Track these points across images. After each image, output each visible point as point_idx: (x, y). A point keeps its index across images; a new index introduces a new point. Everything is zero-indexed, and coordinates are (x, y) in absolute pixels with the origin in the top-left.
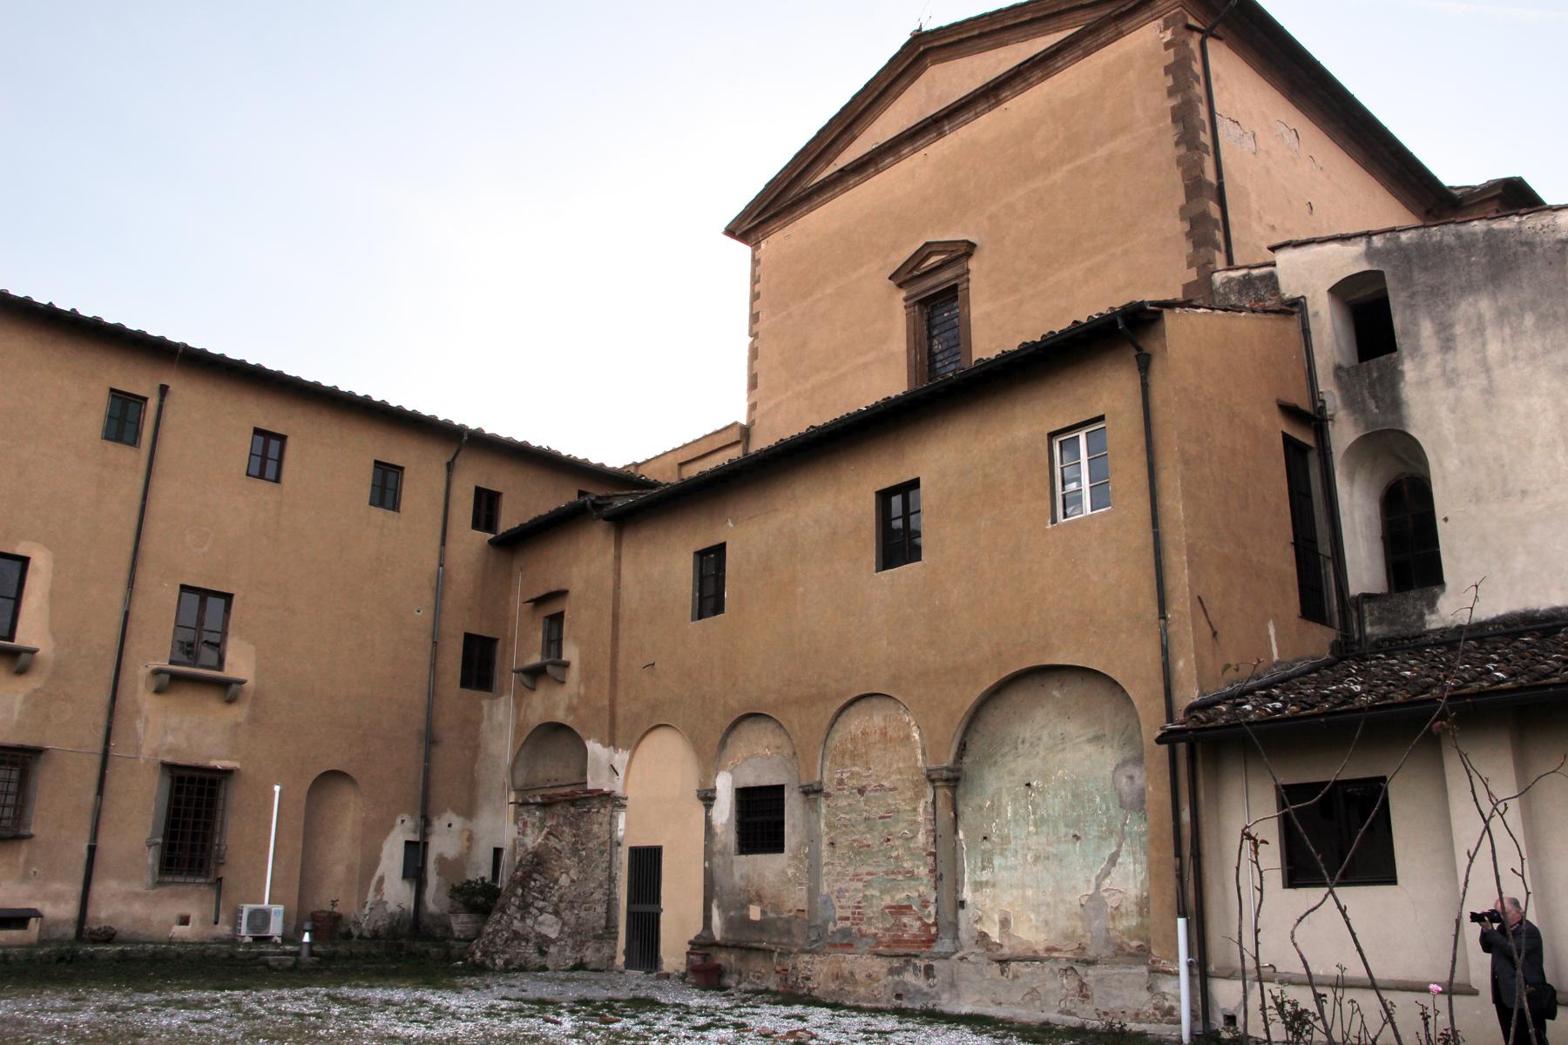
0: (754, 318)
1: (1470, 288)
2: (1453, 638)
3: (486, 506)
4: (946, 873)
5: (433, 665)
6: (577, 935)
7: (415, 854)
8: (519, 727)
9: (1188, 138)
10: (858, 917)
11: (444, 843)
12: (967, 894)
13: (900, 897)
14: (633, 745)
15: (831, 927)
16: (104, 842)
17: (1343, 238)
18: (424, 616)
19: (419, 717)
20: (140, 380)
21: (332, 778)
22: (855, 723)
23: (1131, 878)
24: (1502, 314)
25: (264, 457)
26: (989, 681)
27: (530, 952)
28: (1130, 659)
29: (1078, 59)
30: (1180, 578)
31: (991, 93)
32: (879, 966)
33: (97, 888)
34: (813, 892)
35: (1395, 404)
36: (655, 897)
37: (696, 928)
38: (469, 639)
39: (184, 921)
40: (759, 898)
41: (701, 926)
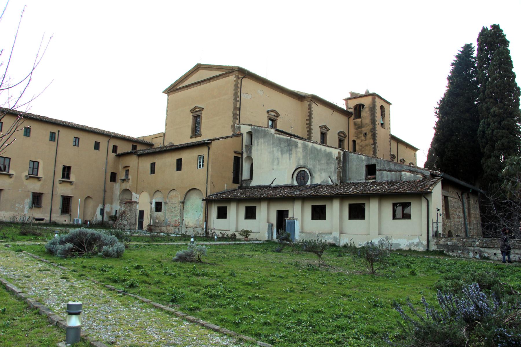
0: (167, 111)
1: (261, 138)
2: (254, 187)
3: (115, 149)
4: (182, 216)
5: (105, 178)
6: (130, 224)
7: (102, 211)
8: (120, 189)
9: (236, 100)
10: (171, 221)
11: (107, 209)
12: (184, 219)
13: (176, 219)
14: (140, 194)
16: (53, 208)
17: (249, 125)
18: (104, 169)
19: (103, 188)
20: (55, 129)
21: (88, 197)
22: (172, 193)
23: (202, 217)
24: (264, 142)
25: (76, 142)
26: (188, 189)
27: (122, 226)
28: (203, 189)
30: (209, 179)
31: (209, 80)
32: (172, 228)
33: (52, 215)
34: (165, 218)
35: (251, 152)
36: (143, 219)
38: (112, 173)
39: (65, 221)
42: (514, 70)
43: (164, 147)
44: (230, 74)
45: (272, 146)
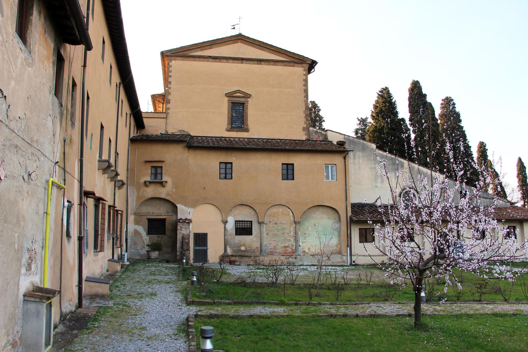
4: (296, 240)
10: (275, 248)
13: (286, 245)
15: (267, 251)
22: (274, 210)
24: (363, 156)
29: (283, 66)
31: (260, 61)
36: (205, 244)
37: (222, 252)
40: (244, 245)
41: (223, 252)
42: (409, 114)
43: (167, 134)
44: (296, 65)
45: (373, 162)
